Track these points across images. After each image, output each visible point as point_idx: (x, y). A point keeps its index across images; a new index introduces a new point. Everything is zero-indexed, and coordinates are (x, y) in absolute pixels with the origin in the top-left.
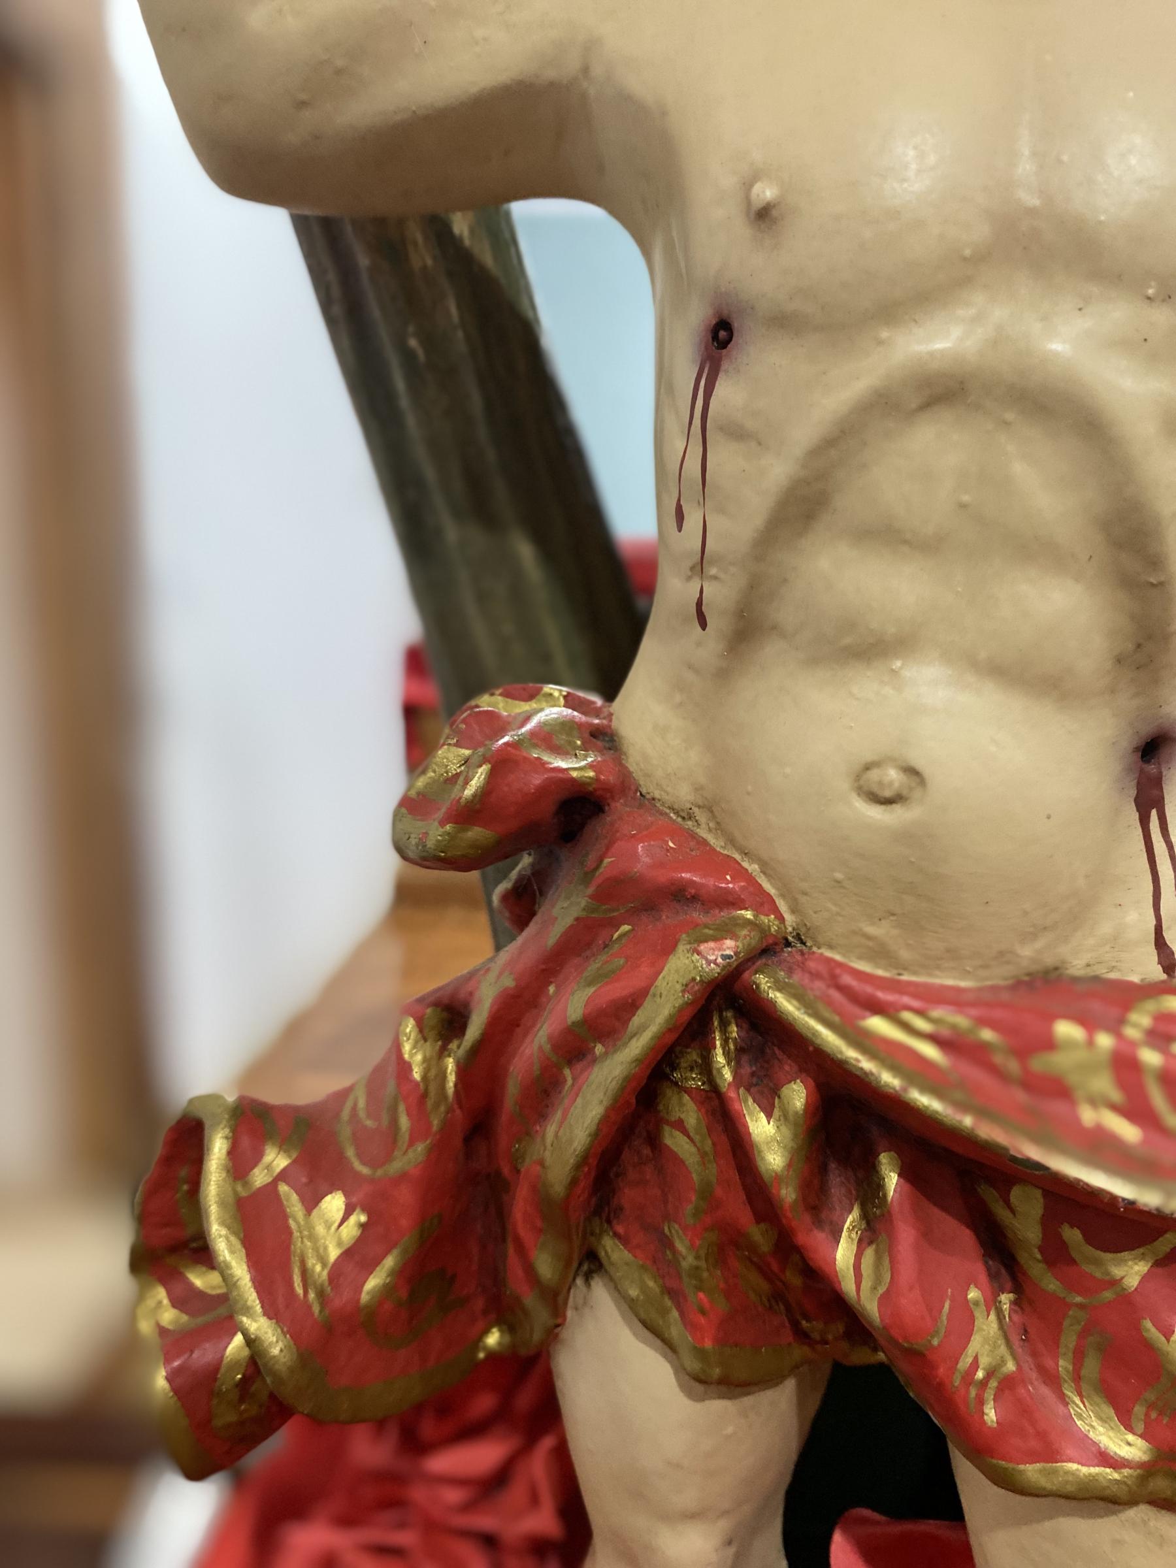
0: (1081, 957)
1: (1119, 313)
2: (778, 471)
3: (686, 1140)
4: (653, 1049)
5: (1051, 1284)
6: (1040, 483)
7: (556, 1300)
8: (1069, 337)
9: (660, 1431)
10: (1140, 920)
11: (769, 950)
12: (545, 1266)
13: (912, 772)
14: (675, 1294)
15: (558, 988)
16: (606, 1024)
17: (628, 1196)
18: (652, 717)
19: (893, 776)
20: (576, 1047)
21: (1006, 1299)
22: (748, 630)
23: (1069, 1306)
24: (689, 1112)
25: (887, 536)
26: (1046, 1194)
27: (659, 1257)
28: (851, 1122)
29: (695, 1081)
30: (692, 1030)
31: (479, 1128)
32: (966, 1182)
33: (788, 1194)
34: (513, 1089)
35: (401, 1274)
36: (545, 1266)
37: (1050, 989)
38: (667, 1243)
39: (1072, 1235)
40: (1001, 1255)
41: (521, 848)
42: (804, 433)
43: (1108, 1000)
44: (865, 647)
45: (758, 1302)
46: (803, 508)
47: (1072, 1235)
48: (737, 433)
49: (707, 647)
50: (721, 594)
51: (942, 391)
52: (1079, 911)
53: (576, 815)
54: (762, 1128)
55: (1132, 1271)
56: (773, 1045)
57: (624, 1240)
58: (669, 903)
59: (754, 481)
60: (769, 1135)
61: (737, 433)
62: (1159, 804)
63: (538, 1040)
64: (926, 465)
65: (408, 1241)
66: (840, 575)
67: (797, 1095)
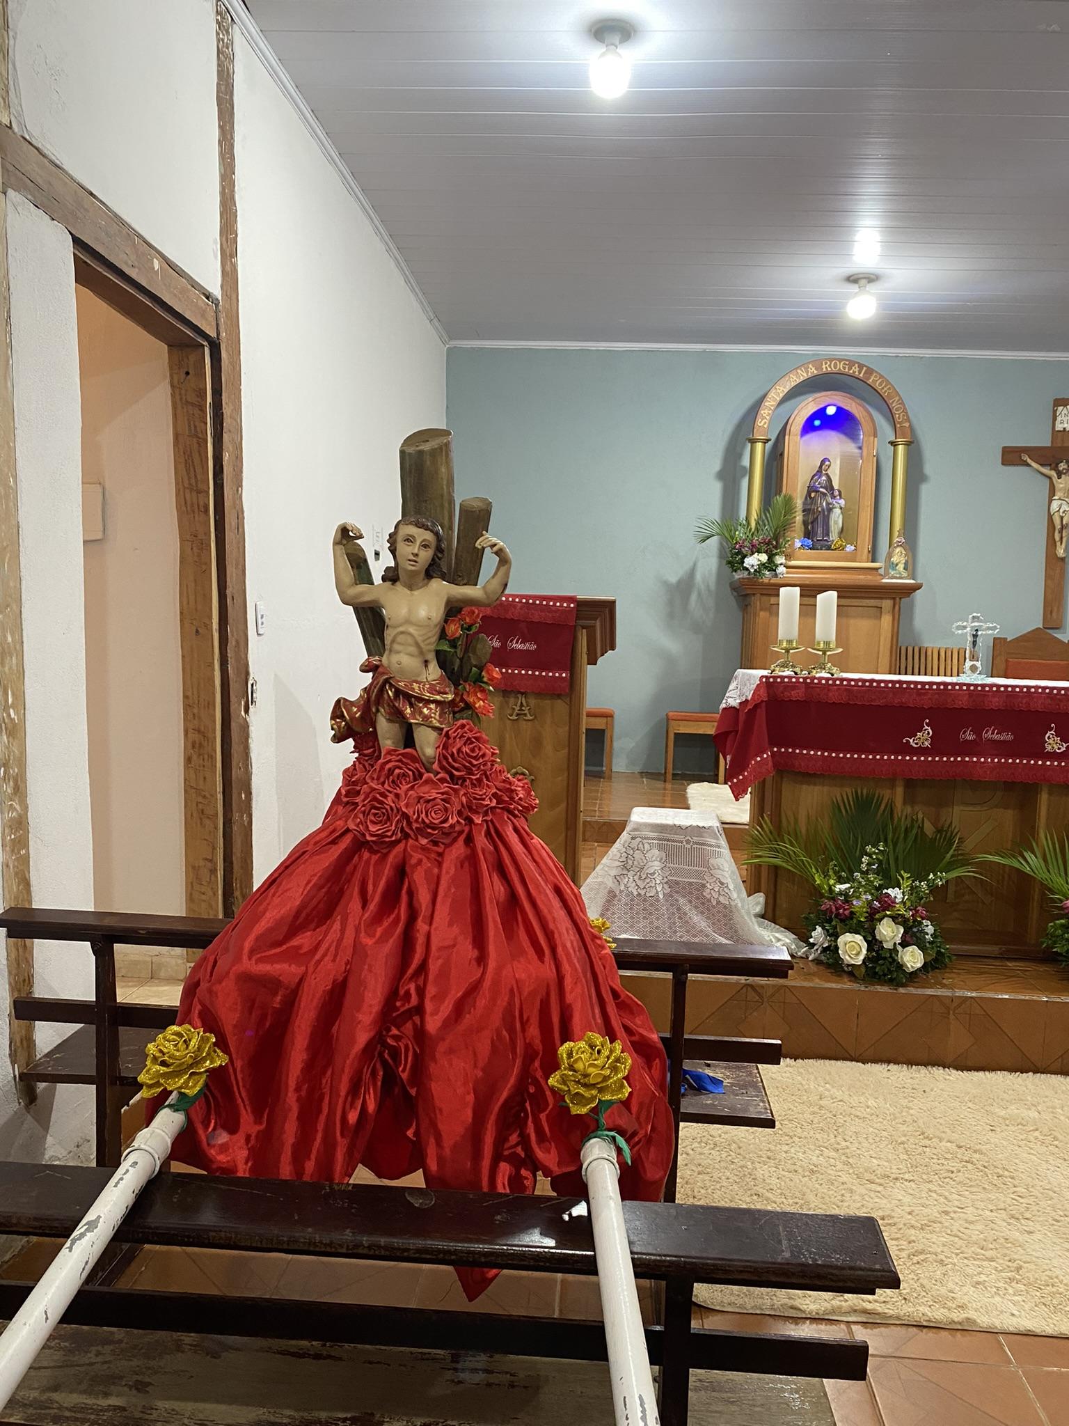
6: (410, 640)
7: (375, 714)
8: (411, 630)
9: (386, 730)
18: (384, 659)
28: (398, 692)
31: (369, 698)
32: (408, 697)
40: (411, 705)
44: (398, 652)
45: (397, 716)
46: (393, 641)
51: (402, 633)
52: (419, 675)
53: (377, 667)
58: (384, 673)
64: (401, 638)
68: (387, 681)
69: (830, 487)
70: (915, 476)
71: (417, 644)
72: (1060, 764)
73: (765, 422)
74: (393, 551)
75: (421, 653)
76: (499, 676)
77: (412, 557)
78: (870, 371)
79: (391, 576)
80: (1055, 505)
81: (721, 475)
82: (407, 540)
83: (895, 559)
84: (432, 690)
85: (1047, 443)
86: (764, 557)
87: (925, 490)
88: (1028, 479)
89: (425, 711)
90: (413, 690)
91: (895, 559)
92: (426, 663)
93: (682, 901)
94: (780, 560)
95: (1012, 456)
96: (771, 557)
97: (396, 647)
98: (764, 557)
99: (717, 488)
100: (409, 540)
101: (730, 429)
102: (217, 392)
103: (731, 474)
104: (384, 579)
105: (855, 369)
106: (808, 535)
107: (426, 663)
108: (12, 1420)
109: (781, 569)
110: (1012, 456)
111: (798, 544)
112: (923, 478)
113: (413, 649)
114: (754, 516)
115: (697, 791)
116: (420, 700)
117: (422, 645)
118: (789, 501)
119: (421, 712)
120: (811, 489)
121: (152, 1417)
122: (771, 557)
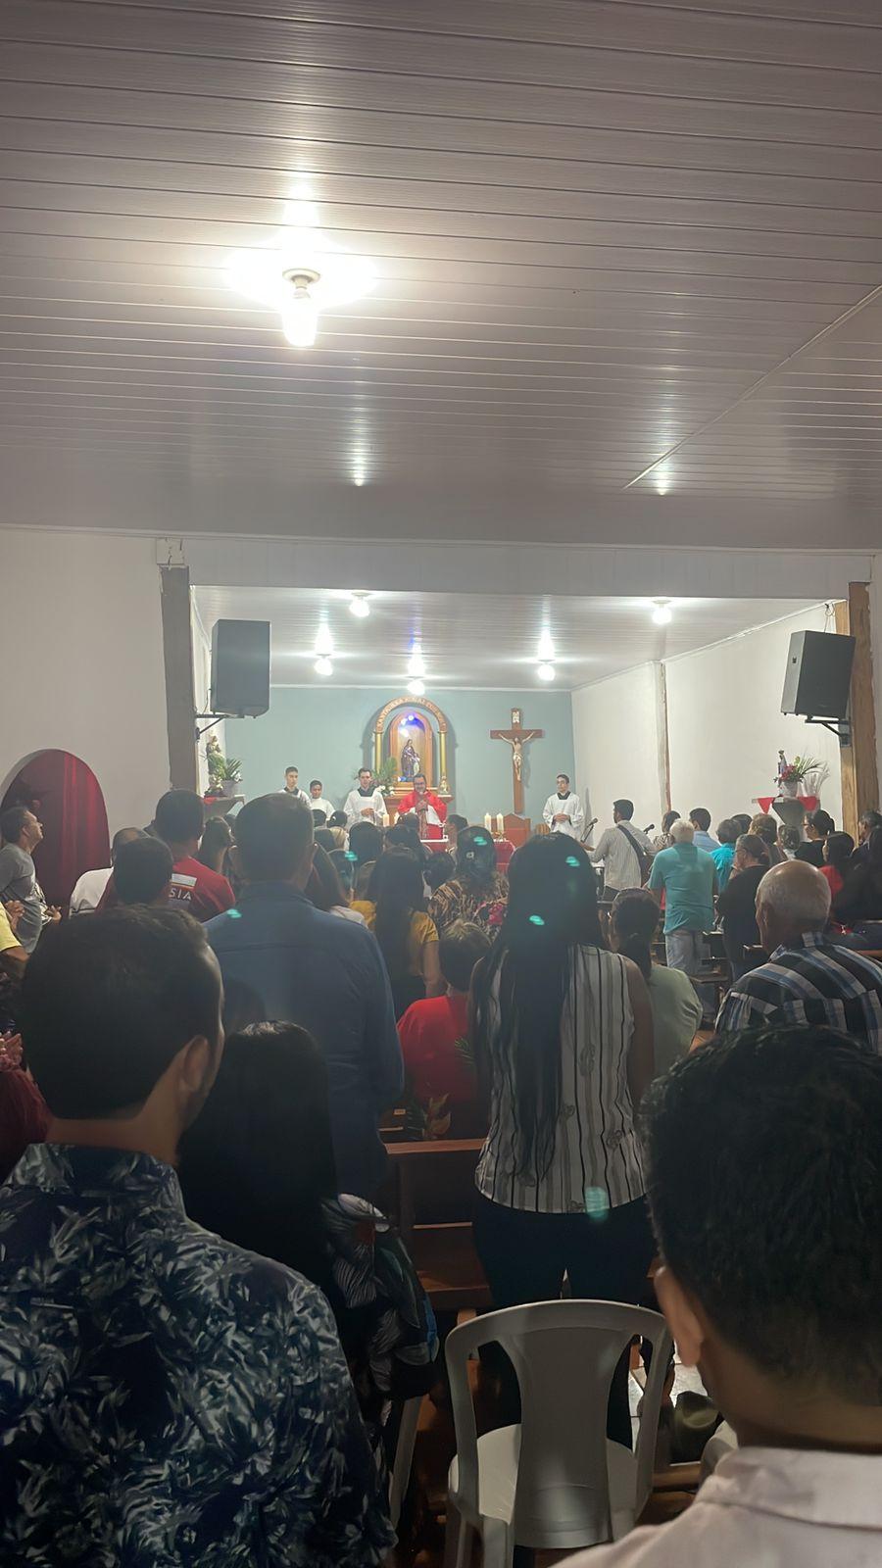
32: (193, 1418)
69: (413, 752)
70: (451, 744)
73: (382, 723)
78: (427, 701)
80: (515, 757)
81: (362, 746)
83: (443, 786)
85: (509, 728)
86: (384, 788)
87: (457, 750)
88: (502, 744)
91: (443, 786)
93: (57, 1535)
94: (391, 788)
95: (495, 734)
96: (387, 787)
98: (384, 788)
99: (360, 753)
101: (365, 724)
103: (367, 745)
105: (420, 701)
106: (404, 775)
108: (203, 1231)
109: (392, 792)
110: (495, 734)
111: (399, 779)
112: (455, 745)
114: (378, 768)
115: (88, 1499)
118: (394, 759)
120: (404, 753)
121: (341, 1541)
122: (387, 787)
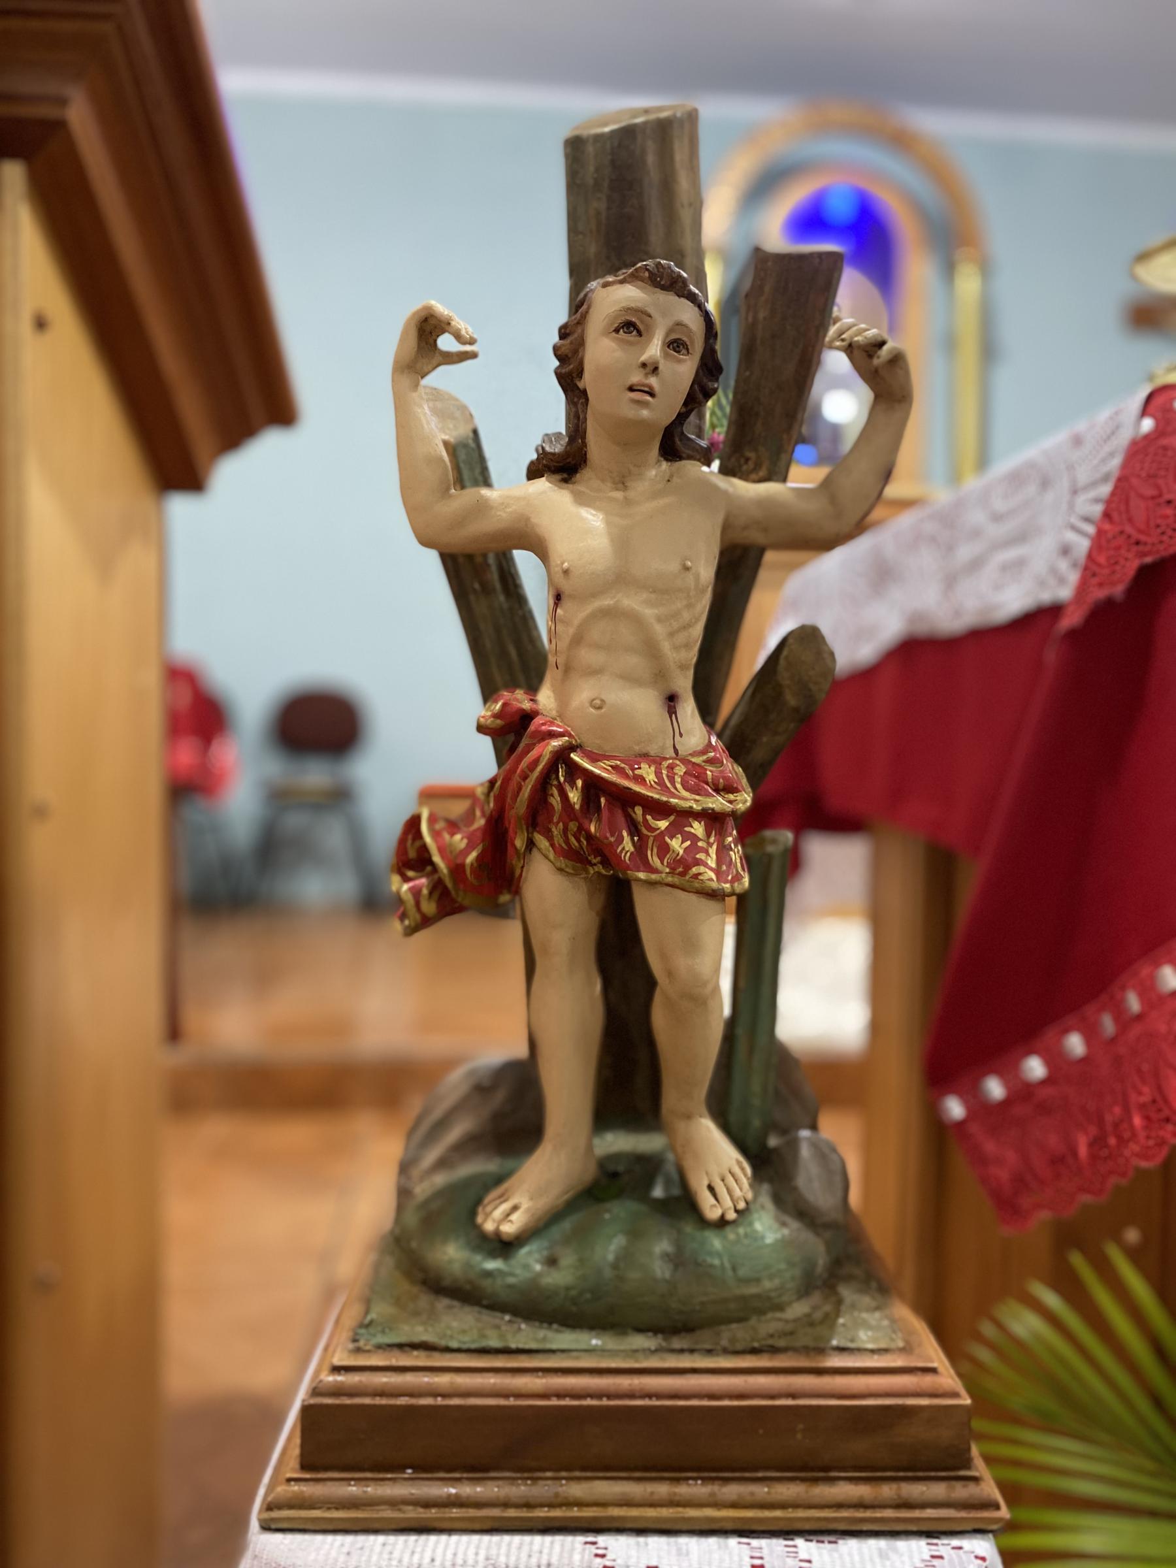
0: (653, 750)
1: (645, 595)
2: (571, 631)
3: (555, 800)
4: (541, 773)
5: (645, 831)
8: (632, 601)
10: (670, 743)
11: (572, 748)
12: (520, 843)
13: (602, 701)
14: (552, 845)
15: (510, 1321)
16: (536, 762)
17: (541, 819)
18: (546, 698)
19: (598, 702)
20: (525, 777)
21: (636, 838)
22: (568, 670)
23: (648, 837)
24: (555, 792)
25: (597, 646)
26: (643, 807)
27: (550, 838)
28: (594, 786)
29: (555, 783)
30: (552, 769)
32: (625, 800)
33: (577, 807)
34: (509, 795)
35: (478, 858)
36: (520, 843)
37: (645, 756)
38: (550, 830)
39: (649, 817)
41: (510, 732)
42: (576, 622)
43: (656, 761)
44: (594, 672)
46: (577, 640)
47: (649, 817)
48: (562, 621)
49: (558, 674)
50: (561, 660)
54: (571, 795)
55: (663, 824)
56: (574, 771)
57: (539, 832)
59: (567, 633)
60: (574, 796)
61: (562, 621)
62: (675, 713)
63: (516, 777)
65: (480, 848)
66: (587, 656)
67: (579, 783)
68: (561, 756)
71: (651, 649)
72: (1055, 1059)
74: (570, 376)
75: (660, 675)
76: (727, 843)
77: (636, 378)
79: (561, 464)
82: (628, 326)
84: (696, 780)
89: (677, 845)
90: (640, 780)
92: (671, 700)
97: (587, 656)
100: (630, 326)
102: (390, 1479)
104: (534, 472)
107: (671, 700)
113: (634, 662)
116: (661, 809)
117: (666, 647)
119: (664, 849)
